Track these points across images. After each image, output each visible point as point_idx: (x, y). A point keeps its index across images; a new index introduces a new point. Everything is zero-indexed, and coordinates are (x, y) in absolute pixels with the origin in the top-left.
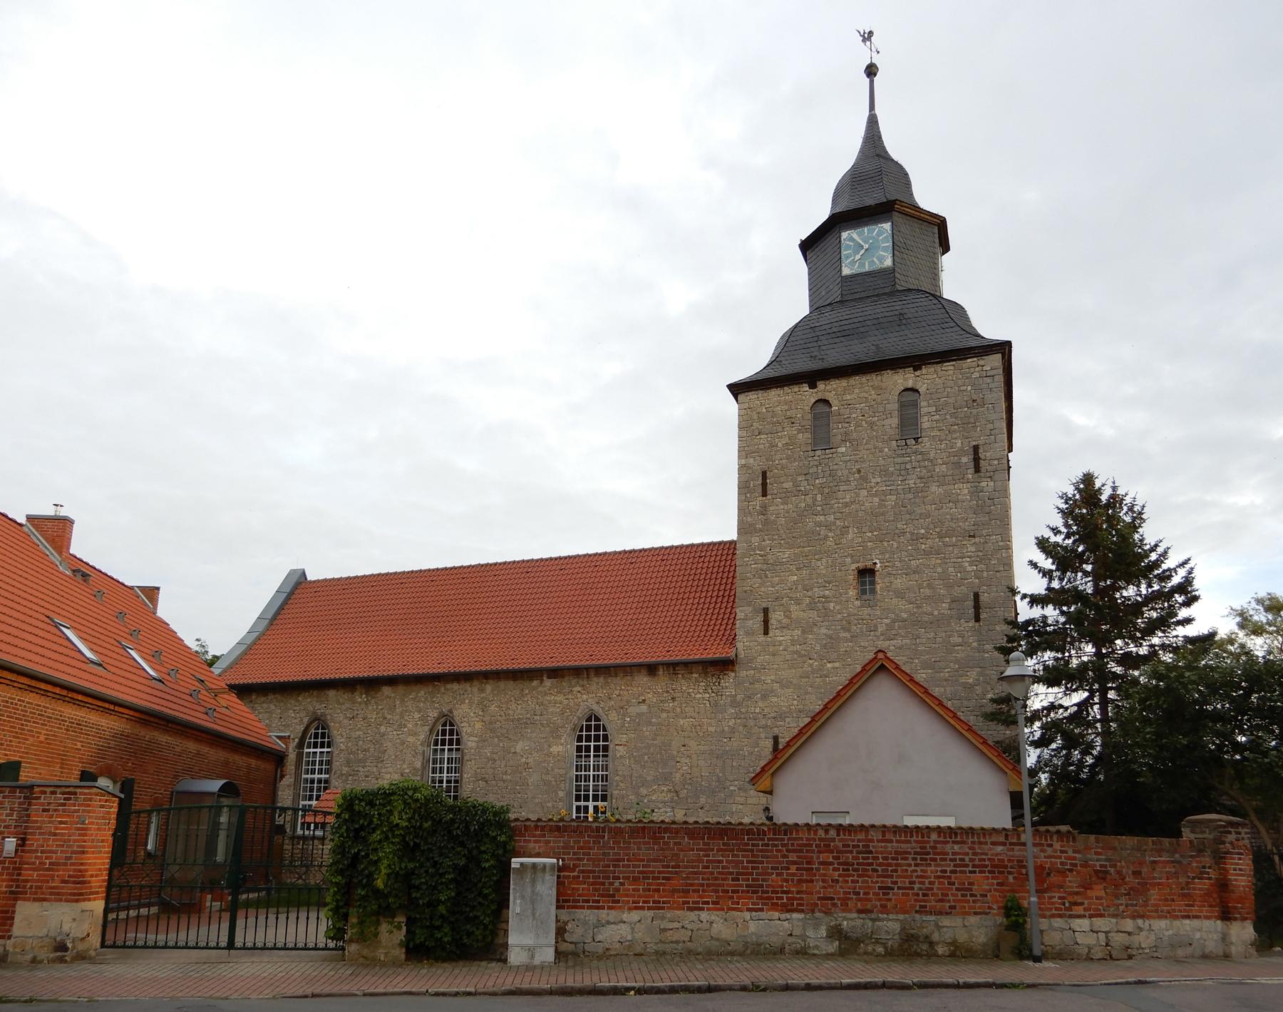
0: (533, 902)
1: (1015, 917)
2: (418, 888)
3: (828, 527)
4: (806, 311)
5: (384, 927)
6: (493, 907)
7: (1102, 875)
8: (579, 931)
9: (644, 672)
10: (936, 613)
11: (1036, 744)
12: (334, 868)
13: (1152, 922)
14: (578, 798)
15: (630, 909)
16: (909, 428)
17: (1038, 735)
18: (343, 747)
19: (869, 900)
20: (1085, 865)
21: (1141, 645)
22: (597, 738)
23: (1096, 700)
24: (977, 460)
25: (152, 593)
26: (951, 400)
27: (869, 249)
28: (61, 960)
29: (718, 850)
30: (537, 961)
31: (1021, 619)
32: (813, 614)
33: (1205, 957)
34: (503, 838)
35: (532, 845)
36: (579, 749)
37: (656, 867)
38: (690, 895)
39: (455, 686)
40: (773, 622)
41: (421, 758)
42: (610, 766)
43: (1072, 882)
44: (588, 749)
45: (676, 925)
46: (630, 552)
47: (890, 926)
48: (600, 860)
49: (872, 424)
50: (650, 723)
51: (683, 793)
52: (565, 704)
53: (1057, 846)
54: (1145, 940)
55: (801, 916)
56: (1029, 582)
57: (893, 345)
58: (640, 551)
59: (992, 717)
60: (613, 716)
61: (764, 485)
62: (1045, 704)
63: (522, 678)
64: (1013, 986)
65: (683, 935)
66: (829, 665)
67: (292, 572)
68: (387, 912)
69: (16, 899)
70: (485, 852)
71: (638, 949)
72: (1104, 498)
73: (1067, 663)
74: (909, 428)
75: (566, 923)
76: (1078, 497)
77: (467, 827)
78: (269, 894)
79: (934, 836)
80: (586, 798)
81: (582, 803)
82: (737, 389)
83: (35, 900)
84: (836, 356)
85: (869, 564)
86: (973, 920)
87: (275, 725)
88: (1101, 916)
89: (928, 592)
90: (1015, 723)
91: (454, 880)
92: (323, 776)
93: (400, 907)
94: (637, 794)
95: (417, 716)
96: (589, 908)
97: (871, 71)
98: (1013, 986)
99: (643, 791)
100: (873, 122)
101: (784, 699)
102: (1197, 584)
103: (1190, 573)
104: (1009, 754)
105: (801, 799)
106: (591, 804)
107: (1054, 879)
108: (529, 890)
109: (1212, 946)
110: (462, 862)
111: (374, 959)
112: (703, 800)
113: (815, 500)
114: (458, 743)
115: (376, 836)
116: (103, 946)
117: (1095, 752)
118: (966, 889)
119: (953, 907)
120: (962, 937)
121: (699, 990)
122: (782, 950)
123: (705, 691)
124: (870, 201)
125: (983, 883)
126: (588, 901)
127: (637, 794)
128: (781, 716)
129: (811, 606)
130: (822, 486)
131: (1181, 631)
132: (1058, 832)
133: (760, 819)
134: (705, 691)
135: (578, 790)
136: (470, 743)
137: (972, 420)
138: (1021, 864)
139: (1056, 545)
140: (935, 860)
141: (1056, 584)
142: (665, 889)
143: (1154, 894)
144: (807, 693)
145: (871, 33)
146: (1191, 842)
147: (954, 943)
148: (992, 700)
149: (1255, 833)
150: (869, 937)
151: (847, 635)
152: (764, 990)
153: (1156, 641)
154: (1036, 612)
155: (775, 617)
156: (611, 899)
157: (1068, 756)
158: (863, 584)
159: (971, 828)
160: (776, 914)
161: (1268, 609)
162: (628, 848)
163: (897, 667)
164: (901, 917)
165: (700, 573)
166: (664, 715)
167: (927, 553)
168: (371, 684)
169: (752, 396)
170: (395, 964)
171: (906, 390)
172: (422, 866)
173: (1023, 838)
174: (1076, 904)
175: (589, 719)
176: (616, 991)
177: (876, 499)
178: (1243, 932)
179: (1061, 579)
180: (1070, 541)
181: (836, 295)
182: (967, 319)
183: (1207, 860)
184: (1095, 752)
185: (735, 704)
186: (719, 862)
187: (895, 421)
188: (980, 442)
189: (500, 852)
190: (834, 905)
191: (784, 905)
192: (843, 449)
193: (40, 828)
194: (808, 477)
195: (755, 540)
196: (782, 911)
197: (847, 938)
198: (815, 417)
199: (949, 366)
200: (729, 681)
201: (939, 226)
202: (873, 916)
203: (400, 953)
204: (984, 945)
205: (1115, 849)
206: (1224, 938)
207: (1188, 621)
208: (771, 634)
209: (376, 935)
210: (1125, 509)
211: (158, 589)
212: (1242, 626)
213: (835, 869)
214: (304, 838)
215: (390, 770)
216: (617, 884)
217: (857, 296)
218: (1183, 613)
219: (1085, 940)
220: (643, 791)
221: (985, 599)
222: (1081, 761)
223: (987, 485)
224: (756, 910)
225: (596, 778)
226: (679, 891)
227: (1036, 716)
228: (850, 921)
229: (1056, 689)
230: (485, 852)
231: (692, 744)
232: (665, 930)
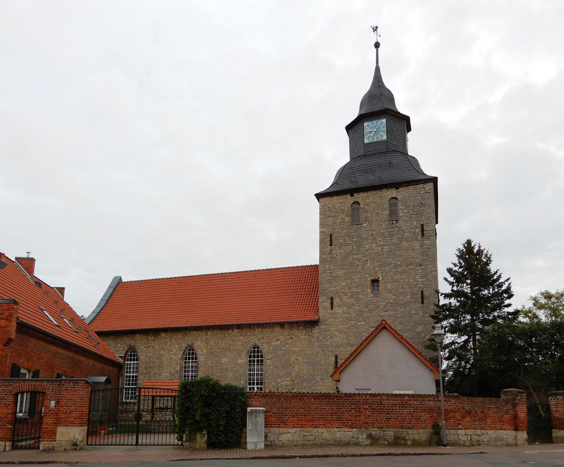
0: (256, 425)
1: (437, 431)
2: (212, 420)
3: (359, 260)
4: (347, 159)
5: (198, 436)
6: (241, 427)
7: (469, 413)
8: (273, 436)
9: (278, 326)
10: (405, 300)
11: (447, 359)
12: (180, 412)
13: (488, 431)
14: (250, 384)
15: (292, 428)
16: (393, 216)
17: (447, 355)
18: (143, 361)
19: (382, 423)
20: (463, 409)
21: (490, 316)
22: (258, 357)
23: (471, 339)
24: (423, 231)
25: (62, 290)
26: (412, 203)
27: (376, 131)
28: (76, 450)
29: (325, 404)
30: (258, 448)
31: (441, 304)
32: (352, 300)
33: (508, 445)
34: (243, 400)
35: (254, 402)
36: (250, 361)
37: (301, 411)
38: (314, 422)
39: (194, 333)
41: (179, 365)
42: (264, 369)
43: (458, 416)
44: (254, 361)
45: (309, 434)
46: (270, 269)
47: (390, 433)
48: (280, 408)
49: (377, 213)
50: (281, 350)
51: (296, 381)
52: (243, 341)
53: (453, 401)
54: (485, 438)
55: (356, 430)
56: (445, 288)
57: (387, 176)
58: (275, 269)
59: (428, 347)
60: (265, 346)
61: (331, 240)
62: (450, 341)
63: (225, 329)
64: (436, 454)
65: (312, 438)
66: (359, 323)
67: (115, 278)
68: (200, 430)
69: (57, 426)
70: (237, 405)
71: (295, 444)
72: (475, 251)
73: (460, 323)
74: (393, 216)
75: (267, 433)
76: (464, 250)
77: (230, 395)
78: (117, 428)
79: (406, 398)
80: (254, 384)
81: (252, 386)
82: (319, 196)
83: (64, 426)
84: (362, 181)
85: (376, 277)
86: (421, 431)
87: (116, 350)
88: (469, 429)
89: (402, 290)
90: (437, 350)
91: (225, 416)
92: (135, 374)
93: (205, 427)
94: (276, 382)
95: (177, 346)
96: (276, 427)
97: (377, 45)
98: (436, 454)
99: (279, 380)
100: (377, 69)
101: (340, 338)
102: (512, 289)
103: (509, 285)
104: (434, 363)
105: (350, 384)
106: (255, 387)
107: (452, 414)
108: (254, 420)
109: (510, 441)
110: (229, 409)
111: (195, 448)
112: (305, 384)
113: (353, 248)
114: (196, 358)
115: (196, 399)
116: (87, 445)
117: (471, 363)
118: (418, 419)
119: (414, 426)
120: (417, 438)
121: (322, 456)
122: (349, 443)
123: (306, 335)
124: (377, 109)
125: (425, 416)
126: (276, 425)
127: (276, 382)
128: (338, 346)
130: (356, 242)
131: (506, 310)
132: (453, 396)
133: (335, 391)
134: (306, 335)
135: (250, 379)
136: (201, 359)
137: (420, 213)
138: (439, 408)
139: (455, 271)
140: (406, 407)
141: (455, 288)
142: (306, 420)
143: (489, 420)
144: (349, 336)
145: (377, 27)
146: (503, 399)
147: (414, 440)
148: (428, 340)
149: (529, 396)
151: (367, 310)
152: (346, 456)
153: (496, 314)
154: (447, 301)
155: (336, 301)
156: (284, 424)
157: (460, 364)
158: (374, 286)
159: (420, 395)
160: (347, 429)
161: (545, 298)
162: (291, 403)
163: (391, 327)
164: (394, 430)
165: (302, 281)
166: (288, 346)
167: (401, 273)
168: (156, 332)
170: (202, 450)
171: (393, 198)
172: (213, 411)
173: (440, 398)
174: (460, 424)
175: (254, 348)
176: (292, 457)
177: (380, 248)
178: (523, 435)
179: (457, 286)
180: (461, 270)
181: (361, 152)
182: (418, 165)
183: (510, 407)
184: (471, 363)
185: (318, 341)
186: (326, 409)
187: (387, 212)
188: (424, 223)
189: (243, 405)
190: (369, 425)
191: (350, 425)
192: (365, 225)
193: (65, 397)
194: (350, 237)
195: (327, 266)
196: (349, 428)
197: (374, 438)
198: (353, 210)
200: (316, 330)
201: (406, 120)
202: (384, 429)
203: (205, 445)
204: (425, 440)
205: (474, 402)
206: (516, 438)
207: (509, 305)
208: (334, 309)
209: (195, 439)
210: (484, 256)
211: (64, 288)
212: (534, 305)
213: (369, 411)
214: (127, 403)
215: (165, 371)
216: (287, 418)
217: (371, 153)
218: (507, 302)
219: (463, 438)
220: (279, 380)
222: (465, 366)
223: (427, 242)
224: (340, 428)
225: (258, 374)
226: (310, 420)
227: (447, 346)
228: (375, 432)
229: (455, 335)
230: (237, 405)
231: (300, 359)
232: (305, 436)
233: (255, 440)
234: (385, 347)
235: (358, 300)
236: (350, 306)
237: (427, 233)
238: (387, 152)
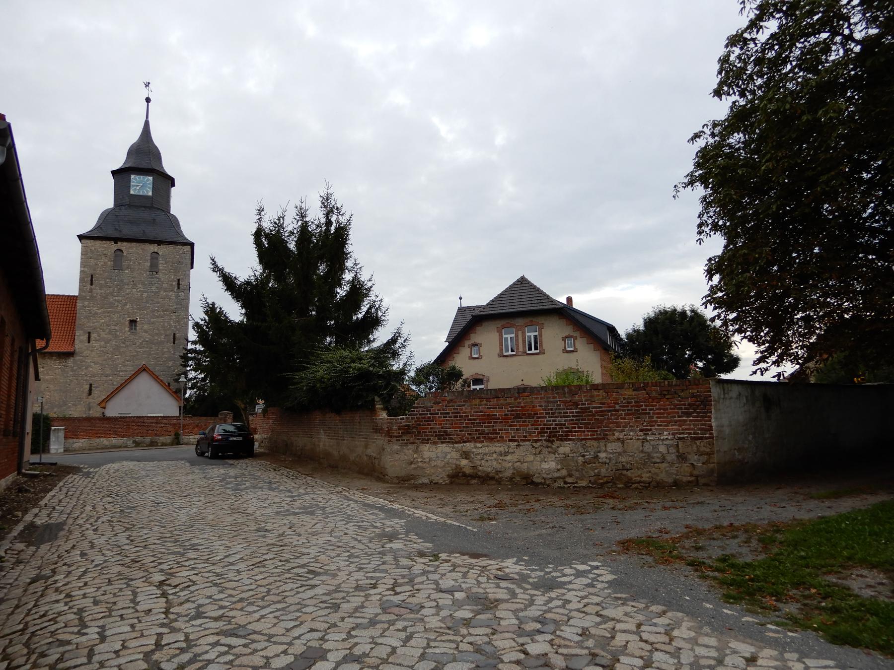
3: (119, 301)
4: (110, 204)
7: (197, 426)
16: (154, 268)
24: (179, 284)
27: (142, 185)
38: (97, 435)
40: (92, 338)
43: (191, 428)
49: (139, 263)
61: (92, 280)
74: (154, 268)
82: (81, 237)
84: (127, 231)
97: (148, 100)
100: (147, 124)
105: (113, 411)
112: (55, 410)
118: (166, 431)
125: (170, 428)
128: (93, 376)
129: (110, 333)
130: (117, 285)
150: (142, 442)
154: (193, 347)
155: (93, 336)
156: (77, 437)
167: (158, 317)
169: (88, 241)
185: (72, 370)
187: (149, 264)
198: (116, 256)
199: (171, 246)
200: (70, 361)
201: (171, 182)
221: (178, 338)
228: (138, 439)
231: (52, 386)
233: (56, 447)
234: (145, 385)
235: (116, 336)
236: (107, 341)
237: (183, 304)
238: (151, 208)
